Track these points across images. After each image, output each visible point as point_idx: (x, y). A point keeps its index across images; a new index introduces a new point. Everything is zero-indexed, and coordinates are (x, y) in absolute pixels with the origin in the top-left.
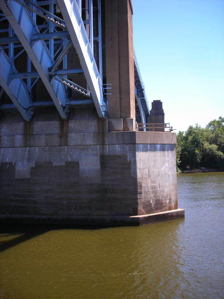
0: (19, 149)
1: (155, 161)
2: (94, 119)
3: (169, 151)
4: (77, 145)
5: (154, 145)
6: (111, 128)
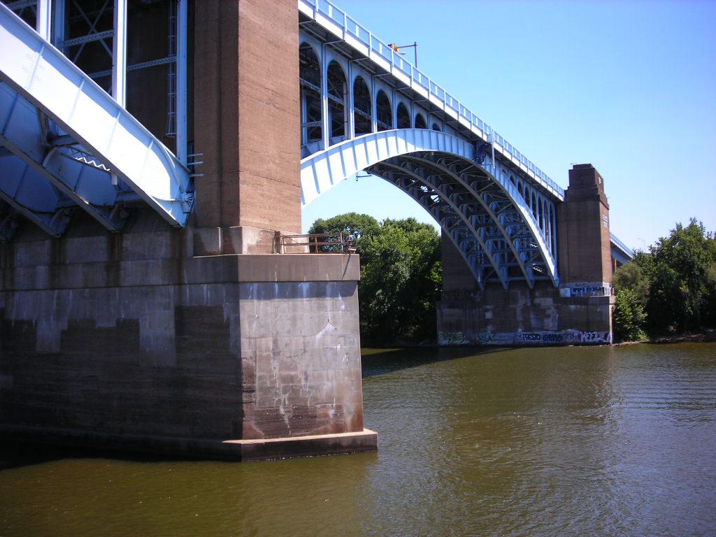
0: (43, 293)
1: (294, 320)
2: (166, 231)
3: (338, 296)
4: (135, 286)
5: (292, 284)
6: (199, 248)
